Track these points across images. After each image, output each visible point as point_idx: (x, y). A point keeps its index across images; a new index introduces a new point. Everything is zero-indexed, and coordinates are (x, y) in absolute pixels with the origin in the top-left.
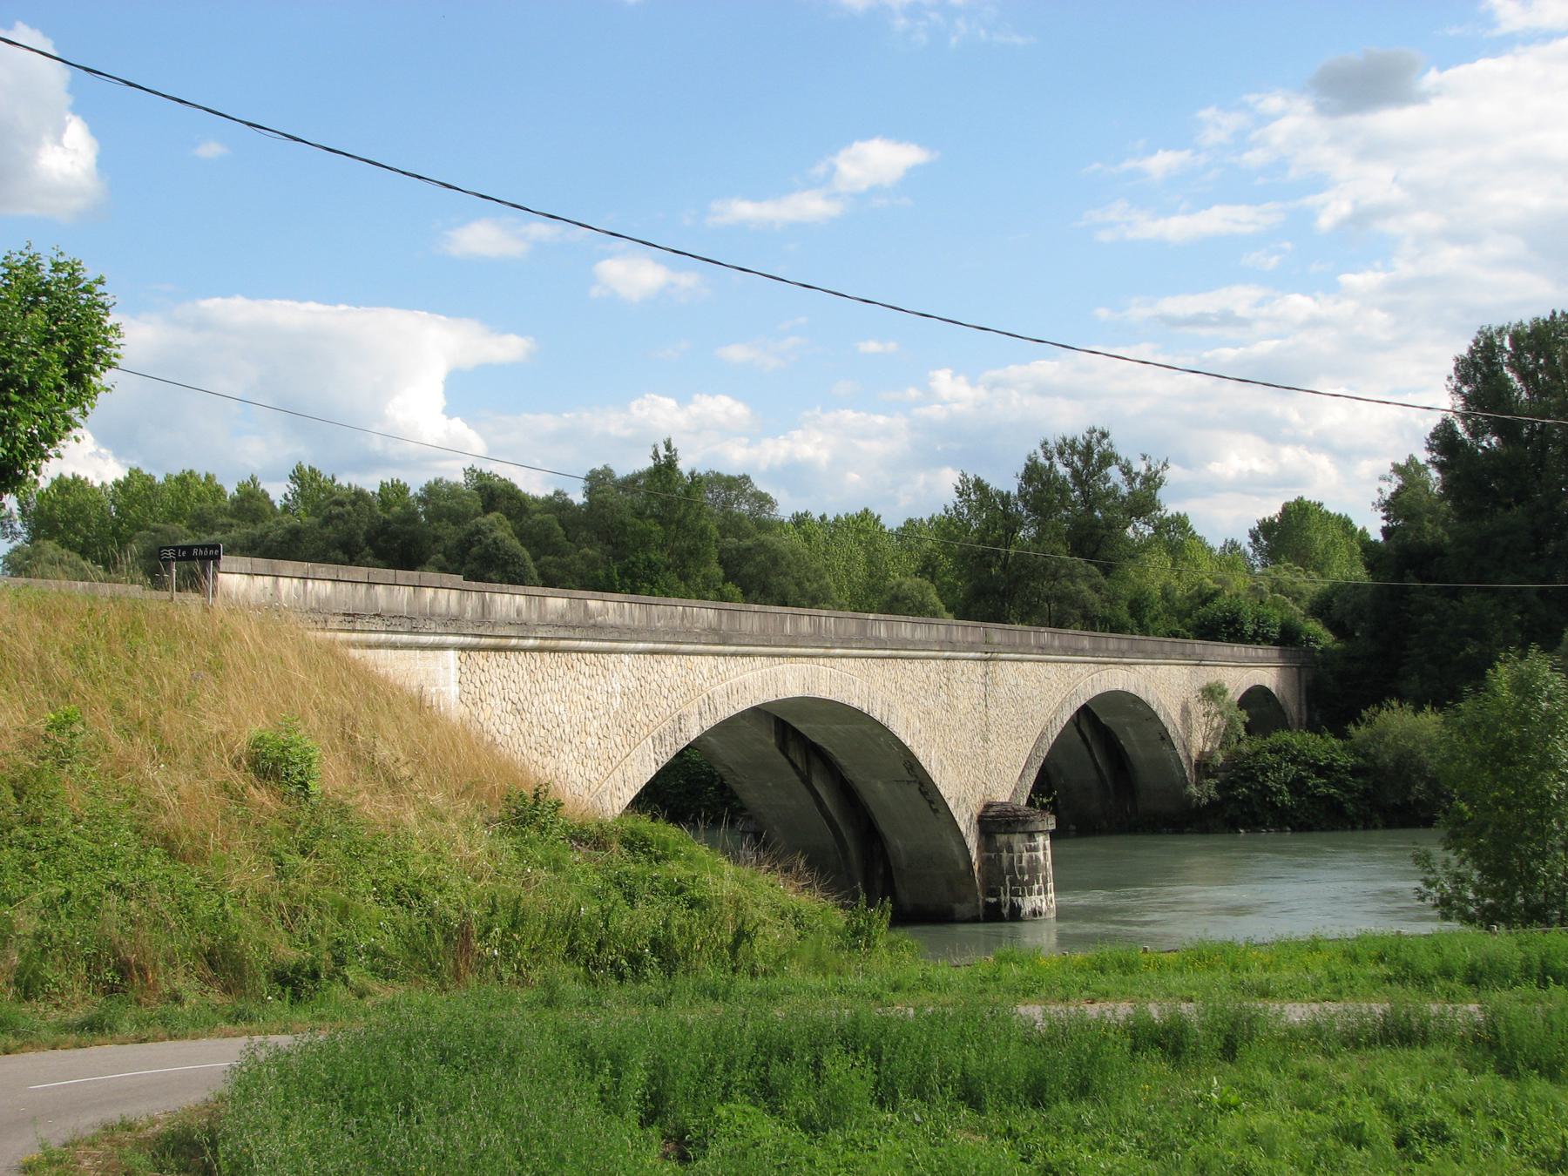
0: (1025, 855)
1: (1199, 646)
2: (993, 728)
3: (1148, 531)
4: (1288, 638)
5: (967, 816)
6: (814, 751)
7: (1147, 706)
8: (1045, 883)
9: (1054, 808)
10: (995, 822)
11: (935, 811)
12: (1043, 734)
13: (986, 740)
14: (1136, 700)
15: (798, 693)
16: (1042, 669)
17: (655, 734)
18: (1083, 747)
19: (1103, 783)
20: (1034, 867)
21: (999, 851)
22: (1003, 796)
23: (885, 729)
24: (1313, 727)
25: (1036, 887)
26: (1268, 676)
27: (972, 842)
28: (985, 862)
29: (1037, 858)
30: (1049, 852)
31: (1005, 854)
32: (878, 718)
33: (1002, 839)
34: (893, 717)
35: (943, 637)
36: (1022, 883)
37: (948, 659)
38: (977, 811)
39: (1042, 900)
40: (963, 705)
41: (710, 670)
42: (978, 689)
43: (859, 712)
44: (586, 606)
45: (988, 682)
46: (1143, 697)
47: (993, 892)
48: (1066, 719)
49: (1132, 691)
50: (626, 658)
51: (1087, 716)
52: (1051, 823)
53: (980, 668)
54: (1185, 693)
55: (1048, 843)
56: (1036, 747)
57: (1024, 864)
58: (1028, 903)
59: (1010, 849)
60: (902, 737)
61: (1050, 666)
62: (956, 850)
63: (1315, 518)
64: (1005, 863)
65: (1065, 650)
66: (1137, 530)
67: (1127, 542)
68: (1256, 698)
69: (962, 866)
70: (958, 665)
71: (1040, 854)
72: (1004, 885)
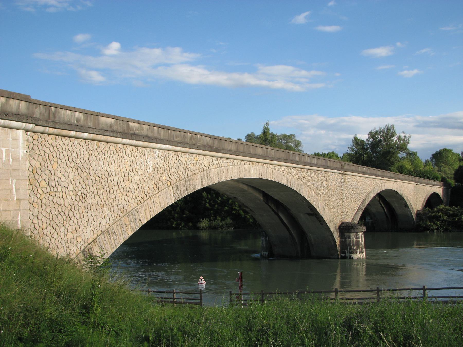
0: (355, 240)
1: (417, 179)
2: (344, 197)
3: (405, 155)
4: (443, 180)
5: (334, 226)
6: (278, 204)
7: (400, 196)
8: (362, 249)
9: (365, 224)
10: (345, 229)
11: (322, 224)
12: (364, 201)
13: (342, 201)
14: (397, 193)
15: (256, 176)
16: (364, 180)
17: (174, 185)
18: (382, 209)
19: (384, 217)
20: (358, 244)
21: (346, 238)
22: (349, 220)
23: (299, 194)
24: (451, 205)
25: (358, 251)
26: (439, 190)
27: (336, 236)
28: (341, 242)
29: (359, 241)
30: (363, 239)
31: (348, 239)
32: (295, 189)
33: (346, 234)
34: (302, 190)
35: (324, 164)
36: (354, 249)
37: (326, 172)
38: (338, 225)
39: (360, 255)
40: (332, 188)
41: (209, 162)
42: (338, 183)
43: (286, 187)
44: (128, 125)
45: (342, 182)
46: (399, 192)
47: (344, 253)
48: (372, 196)
49: (395, 190)
50: (157, 152)
51: (380, 196)
52: (364, 229)
53: (340, 177)
54: (415, 194)
55: (363, 236)
56: (361, 205)
57: (354, 243)
58: (356, 256)
59: (349, 238)
60: (306, 197)
61: (367, 179)
62: (330, 238)
63: (450, 155)
64: (348, 243)
65: (372, 174)
66: (402, 154)
67: (398, 157)
68: (434, 196)
69: (332, 243)
70: (330, 175)
71: (360, 240)
72: (347, 250)
